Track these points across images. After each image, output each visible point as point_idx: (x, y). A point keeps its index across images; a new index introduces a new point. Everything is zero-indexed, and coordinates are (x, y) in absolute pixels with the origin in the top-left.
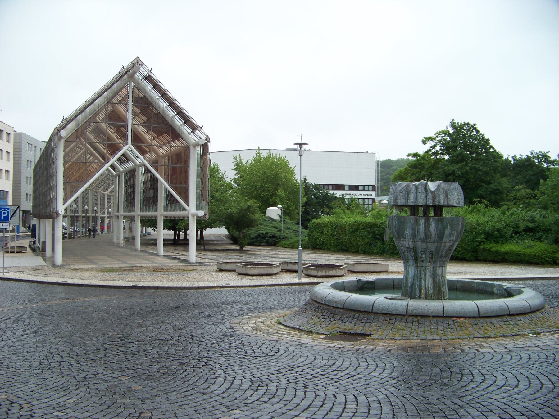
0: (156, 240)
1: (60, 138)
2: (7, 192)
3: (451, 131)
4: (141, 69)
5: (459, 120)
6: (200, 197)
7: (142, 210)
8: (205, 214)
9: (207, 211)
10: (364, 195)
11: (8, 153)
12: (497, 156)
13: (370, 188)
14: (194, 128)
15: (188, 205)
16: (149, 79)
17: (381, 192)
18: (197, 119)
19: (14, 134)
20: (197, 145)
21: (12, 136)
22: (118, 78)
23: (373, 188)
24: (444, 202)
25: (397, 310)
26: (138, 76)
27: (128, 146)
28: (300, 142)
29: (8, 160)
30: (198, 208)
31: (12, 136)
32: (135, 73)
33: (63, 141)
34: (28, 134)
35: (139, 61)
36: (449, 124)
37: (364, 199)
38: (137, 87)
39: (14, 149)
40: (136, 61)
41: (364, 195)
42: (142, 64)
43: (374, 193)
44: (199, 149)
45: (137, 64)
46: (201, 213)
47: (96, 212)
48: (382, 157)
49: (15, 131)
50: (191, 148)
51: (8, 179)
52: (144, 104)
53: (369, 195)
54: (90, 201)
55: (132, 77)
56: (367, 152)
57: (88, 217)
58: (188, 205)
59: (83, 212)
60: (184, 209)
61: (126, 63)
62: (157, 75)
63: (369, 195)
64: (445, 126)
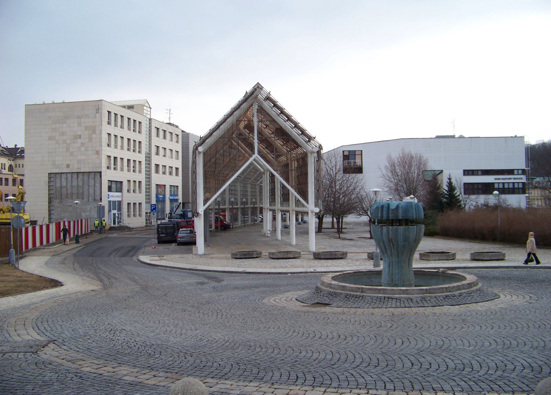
2: (177, 186)
6: (317, 198)
7: (282, 205)
8: (320, 211)
10: (514, 179)
11: (178, 152)
13: (520, 172)
14: (310, 139)
15: (308, 203)
16: (268, 98)
18: (310, 131)
19: (182, 135)
21: (180, 137)
23: (524, 172)
24: (347, 224)
27: (254, 157)
29: (178, 159)
30: (316, 205)
31: (180, 137)
33: (202, 155)
34: (195, 134)
35: (259, 86)
37: (514, 183)
39: (182, 148)
40: (257, 86)
41: (514, 179)
42: (262, 88)
43: (524, 177)
44: (316, 155)
45: (258, 88)
46: (317, 210)
48: (533, 139)
49: (183, 131)
50: (309, 155)
51: (177, 174)
53: (519, 179)
54: (249, 194)
57: (256, 208)
58: (308, 203)
59: (241, 204)
60: (303, 206)
61: (249, 88)
62: (275, 96)
63: (519, 179)
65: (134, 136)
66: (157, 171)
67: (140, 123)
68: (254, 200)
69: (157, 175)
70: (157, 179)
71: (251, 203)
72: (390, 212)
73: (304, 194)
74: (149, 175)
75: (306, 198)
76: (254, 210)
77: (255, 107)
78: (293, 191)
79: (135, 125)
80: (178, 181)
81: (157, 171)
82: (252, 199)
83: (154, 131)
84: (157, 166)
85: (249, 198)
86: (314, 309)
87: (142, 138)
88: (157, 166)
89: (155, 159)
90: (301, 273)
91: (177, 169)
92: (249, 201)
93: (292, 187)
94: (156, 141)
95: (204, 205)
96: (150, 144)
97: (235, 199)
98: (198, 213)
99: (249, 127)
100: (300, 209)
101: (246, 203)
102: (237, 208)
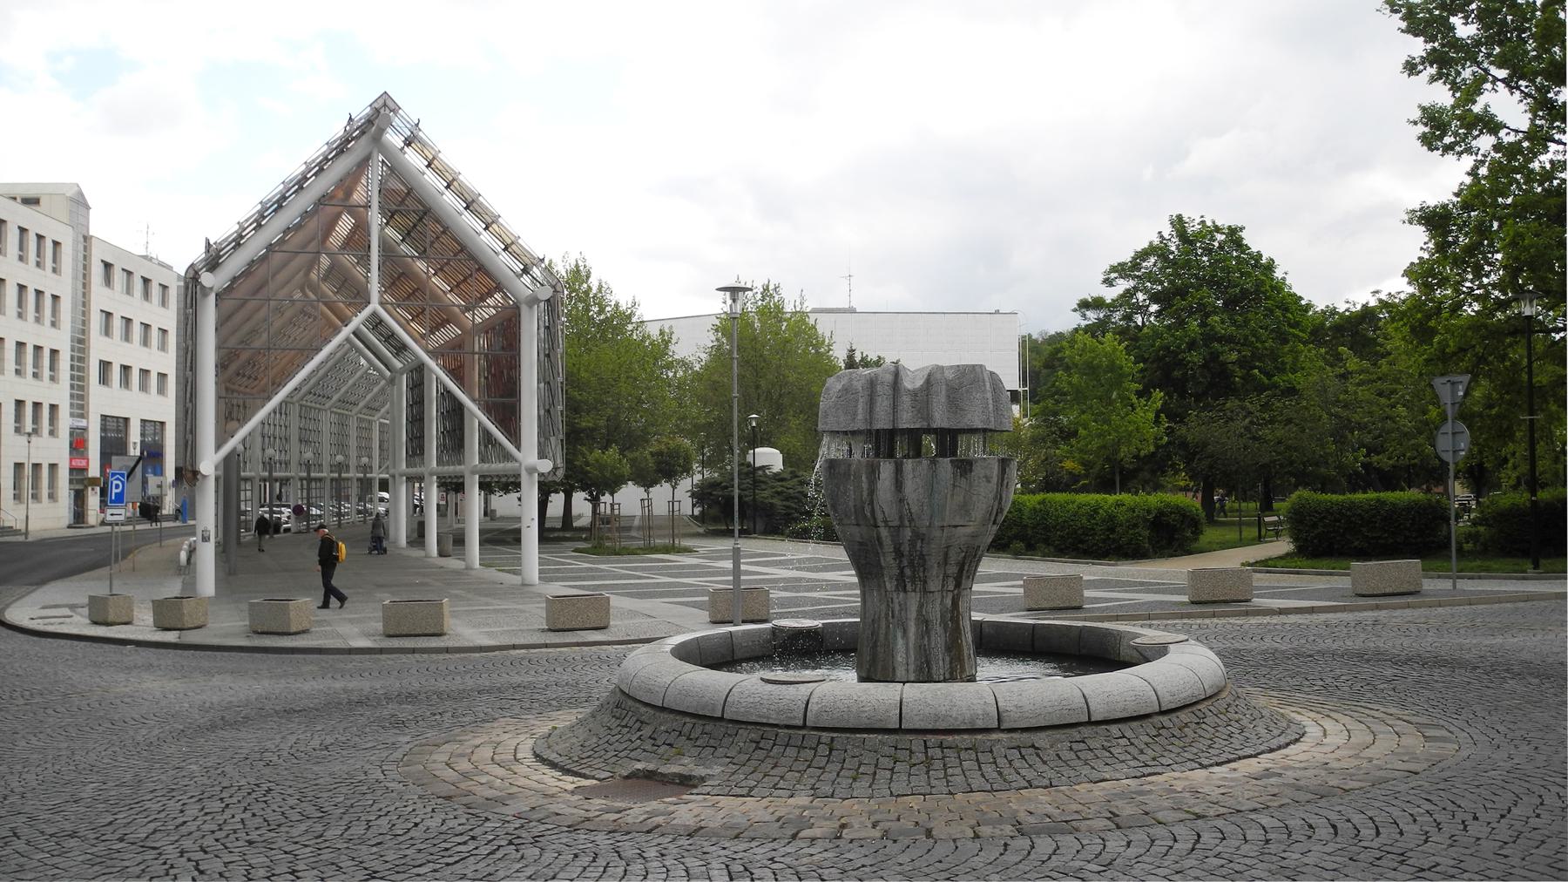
0: (518, 531)
1: (205, 291)
2: (162, 423)
3: (1264, 261)
4: (396, 121)
5: (1196, 214)
8: (555, 468)
9: (559, 461)
11: (164, 332)
12: (1290, 305)
15: (518, 448)
17: (353, 345)
20: (533, 301)
22: (341, 148)
25: (937, 717)
26: (394, 139)
28: (731, 283)
32: (382, 131)
33: (212, 297)
35: (389, 103)
36: (1167, 231)
38: (395, 169)
40: (381, 102)
42: (396, 109)
45: (381, 113)
46: (546, 466)
47: (366, 468)
50: (524, 309)
51: (161, 390)
52: (412, 210)
54: (353, 443)
55: (377, 139)
56: (997, 312)
58: (518, 448)
60: (508, 457)
61: (360, 108)
64: (1149, 229)
65: (36, 278)
66: (104, 379)
67: (56, 244)
68: (365, 460)
69: (103, 389)
70: (105, 400)
71: (359, 467)
72: (906, 401)
73: (508, 417)
74: (81, 388)
75: (514, 434)
76: (365, 485)
77: (376, 172)
78: (477, 417)
79: (45, 250)
80: (164, 408)
81: (104, 379)
82: (359, 457)
83: (97, 271)
84: (105, 366)
85: (353, 453)
86: (638, 810)
87: (63, 285)
88: (105, 366)
89: (100, 347)
90: (514, 647)
91: (162, 376)
92: (353, 463)
93: (474, 400)
94: (101, 298)
95: (218, 447)
96: (85, 304)
97: (317, 454)
98: (195, 473)
99: (358, 240)
100: (497, 467)
101: (340, 467)
102: (320, 480)
